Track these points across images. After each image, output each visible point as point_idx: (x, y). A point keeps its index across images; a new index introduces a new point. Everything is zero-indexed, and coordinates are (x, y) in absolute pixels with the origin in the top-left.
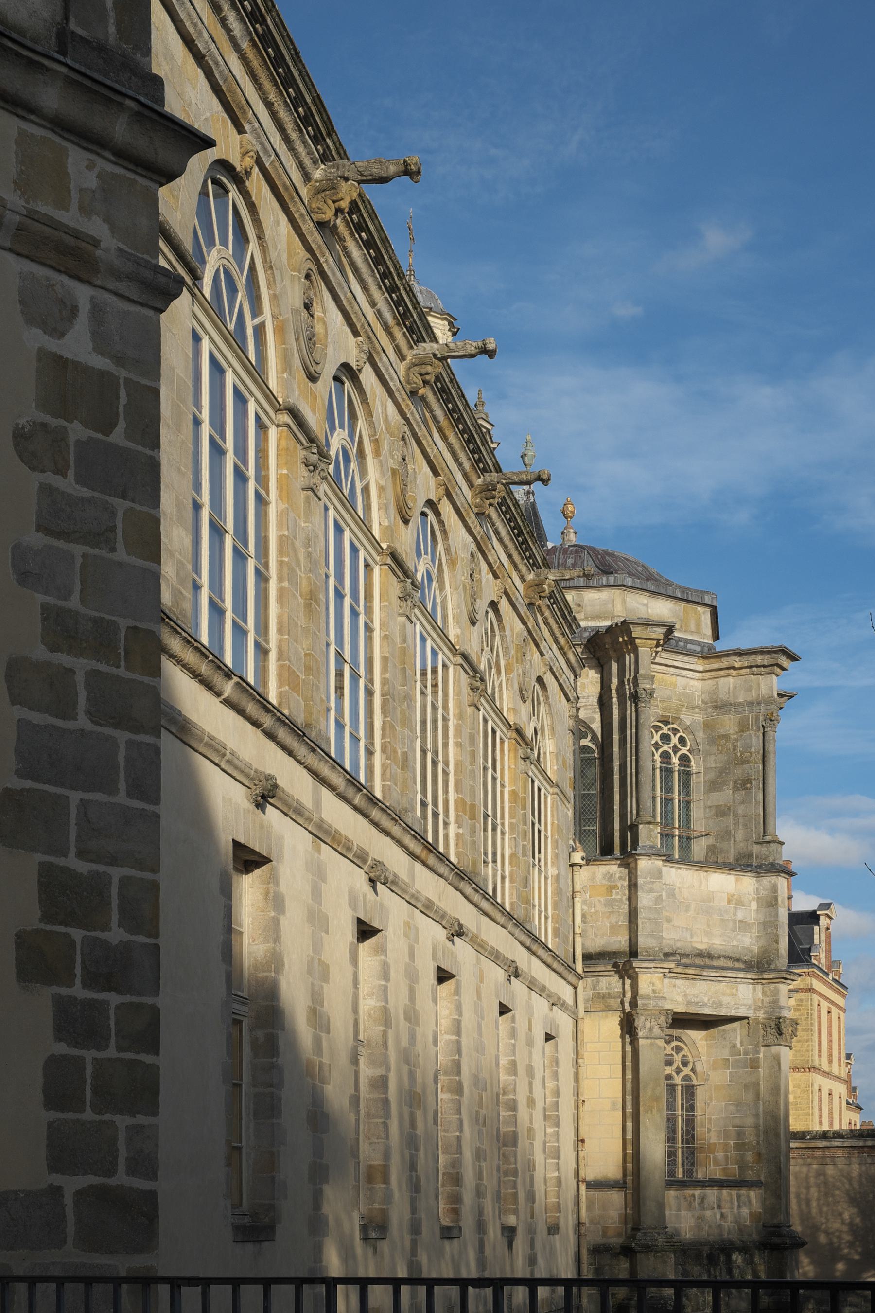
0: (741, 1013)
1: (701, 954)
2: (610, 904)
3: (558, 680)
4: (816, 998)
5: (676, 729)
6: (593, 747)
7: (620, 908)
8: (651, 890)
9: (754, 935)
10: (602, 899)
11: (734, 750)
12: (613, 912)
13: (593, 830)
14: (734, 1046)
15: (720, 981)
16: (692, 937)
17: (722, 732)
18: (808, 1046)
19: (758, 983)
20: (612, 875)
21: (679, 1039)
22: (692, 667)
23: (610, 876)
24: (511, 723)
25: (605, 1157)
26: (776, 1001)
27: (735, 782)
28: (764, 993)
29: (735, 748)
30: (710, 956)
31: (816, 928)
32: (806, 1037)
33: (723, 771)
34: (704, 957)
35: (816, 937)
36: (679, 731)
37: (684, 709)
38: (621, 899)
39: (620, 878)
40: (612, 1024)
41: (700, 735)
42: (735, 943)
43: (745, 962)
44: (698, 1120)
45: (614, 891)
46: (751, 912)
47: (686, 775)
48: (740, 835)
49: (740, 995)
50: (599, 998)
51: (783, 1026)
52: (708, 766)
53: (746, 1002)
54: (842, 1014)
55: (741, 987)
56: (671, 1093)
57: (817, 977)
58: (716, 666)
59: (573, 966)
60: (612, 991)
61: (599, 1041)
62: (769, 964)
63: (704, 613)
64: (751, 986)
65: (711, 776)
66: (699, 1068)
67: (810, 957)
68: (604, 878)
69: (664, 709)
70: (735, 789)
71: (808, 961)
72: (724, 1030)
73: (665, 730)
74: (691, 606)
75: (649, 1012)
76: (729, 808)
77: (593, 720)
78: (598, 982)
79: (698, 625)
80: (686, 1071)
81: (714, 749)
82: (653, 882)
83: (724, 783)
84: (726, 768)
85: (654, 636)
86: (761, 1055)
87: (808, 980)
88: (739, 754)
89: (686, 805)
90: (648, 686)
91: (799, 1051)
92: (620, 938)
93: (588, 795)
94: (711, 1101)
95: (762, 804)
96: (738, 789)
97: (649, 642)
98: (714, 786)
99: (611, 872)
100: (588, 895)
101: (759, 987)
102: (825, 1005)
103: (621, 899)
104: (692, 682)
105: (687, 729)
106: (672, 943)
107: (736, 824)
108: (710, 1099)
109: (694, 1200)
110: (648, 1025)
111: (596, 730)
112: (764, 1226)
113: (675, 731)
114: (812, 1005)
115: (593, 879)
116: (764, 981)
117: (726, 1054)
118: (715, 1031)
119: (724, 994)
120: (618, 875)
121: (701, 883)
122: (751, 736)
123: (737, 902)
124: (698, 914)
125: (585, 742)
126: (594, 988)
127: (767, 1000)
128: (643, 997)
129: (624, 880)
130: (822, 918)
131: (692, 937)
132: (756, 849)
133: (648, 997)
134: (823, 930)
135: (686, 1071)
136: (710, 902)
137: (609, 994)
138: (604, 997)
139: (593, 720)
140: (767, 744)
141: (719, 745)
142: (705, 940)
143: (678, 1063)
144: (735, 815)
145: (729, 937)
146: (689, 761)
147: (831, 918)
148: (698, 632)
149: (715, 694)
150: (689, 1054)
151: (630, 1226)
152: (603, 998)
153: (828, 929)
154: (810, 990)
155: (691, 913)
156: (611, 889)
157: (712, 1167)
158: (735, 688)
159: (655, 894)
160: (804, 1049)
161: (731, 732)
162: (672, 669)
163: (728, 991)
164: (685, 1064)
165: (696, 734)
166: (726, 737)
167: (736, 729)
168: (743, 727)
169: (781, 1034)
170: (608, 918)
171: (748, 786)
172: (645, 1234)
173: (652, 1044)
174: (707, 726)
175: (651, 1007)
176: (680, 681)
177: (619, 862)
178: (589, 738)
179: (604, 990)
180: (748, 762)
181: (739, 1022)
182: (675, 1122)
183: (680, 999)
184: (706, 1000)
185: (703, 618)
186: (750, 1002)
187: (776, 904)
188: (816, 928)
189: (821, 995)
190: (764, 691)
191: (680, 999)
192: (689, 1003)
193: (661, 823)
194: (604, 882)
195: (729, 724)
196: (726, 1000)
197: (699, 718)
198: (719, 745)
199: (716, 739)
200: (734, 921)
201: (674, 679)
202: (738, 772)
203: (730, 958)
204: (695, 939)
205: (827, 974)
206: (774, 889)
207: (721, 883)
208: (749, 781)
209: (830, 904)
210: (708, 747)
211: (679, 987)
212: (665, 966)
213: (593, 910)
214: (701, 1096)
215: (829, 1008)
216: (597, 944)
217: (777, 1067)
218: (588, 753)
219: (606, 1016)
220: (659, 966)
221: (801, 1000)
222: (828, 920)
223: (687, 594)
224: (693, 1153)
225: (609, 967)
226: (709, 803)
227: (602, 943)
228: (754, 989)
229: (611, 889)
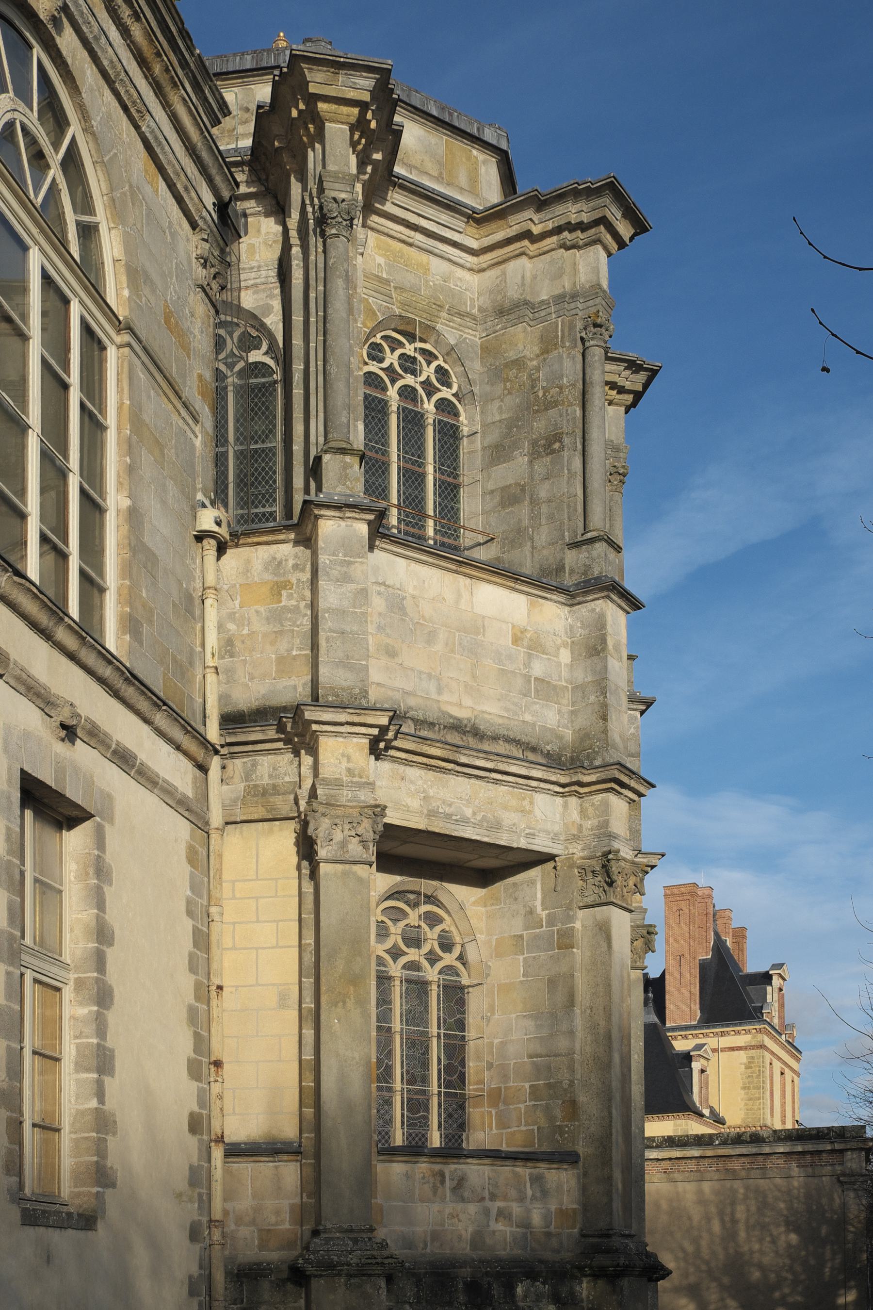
0: (541, 844)
1: (457, 727)
2: (276, 616)
3: (137, 127)
4: (768, 1056)
5: (430, 353)
6: (271, 363)
7: (294, 624)
8: (346, 578)
9: (565, 709)
10: (262, 609)
11: (533, 387)
12: (281, 633)
13: (271, 514)
14: (531, 912)
15: (496, 782)
16: (440, 691)
17: (512, 355)
18: (760, 1104)
19: (571, 794)
20: (280, 563)
21: (430, 899)
22: (456, 237)
23: (277, 565)
24: (121, 318)
25: (258, 1095)
26: (606, 824)
27: (534, 443)
28: (583, 813)
29: (534, 382)
30: (477, 733)
31: (769, 988)
32: (757, 1095)
33: (512, 425)
34: (465, 733)
35: (769, 997)
36: (436, 358)
37: (444, 314)
38: (297, 607)
39: (296, 567)
40: (282, 841)
41: (476, 367)
42: (528, 717)
43: (548, 755)
44: (471, 1047)
45: (284, 593)
46: (561, 663)
47: (449, 436)
48: (543, 536)
49: (538, 813)
50: (255, 795)
51: (614, 868)
52: (489, 420)
53: (549, 827)
54: (796, 1079)
55: (540, 799)
56: (419, 997)
57: (768, 1034)
58: (500, 236)
59: (200, 728)
60: (279, 781)
61: (257, 879)
62: (591, 759)
63: (484, 162)
64: (559, 800)
65: (494, 437)
66: (472, 955)
67: (762, 1014)
68: (266, 569)
69: (404, 305)
70: (534, 455)
71: (759, 1018)
72: (515, 884)
73: (409, 349)
74: (459, 146)
75: (340, 812)
76: (523, 490)
77: (268, 309)
78: (255, 765)
79: (474, 179)
80: (449, 959)
81: (499, 389)
82: (350, 563)
83: (515, 446)
84: (518, 419)
85: (352, 94)
86: (578, 925)
87: (760, 1037)
88: (541, 394)
89: (449, 491)
90: (343, 196)
91: (751, 1109)
92: (294, 681)
93: (263, 450)
94: (493, 1013)
95: (580, 478)
96: (540, 456)
97: (345, 110)
98: (498, 453)
99: (279, 556)
100: (237, 603)
101: (573, 801)
102: (777, 1065)
103: (297, 607)
104: (460, 273)
105: (450, 351)
106: (397, 696)
107: (535, 517)
108: (492, 1009)
109: (443, 1182)
110: (338, 836)
111: (272, 328)
112: (583, 1236)
113: (430, 357)
114: (763, 1062)
115: (247, 571)
116: (582, 790)
117: (517, 926)
118: (499, 887)
119: (505, 808)
120: (291, 563)
121: (459, 596)
122: (560, 357)
123: (532, 644)
124: (453, 651)
125: (256, 356)
126: (247, 777)
127: (588, 824)
128: (327, 782)
129: (303, 570)
130: (775, 978)
131: (440, 691)
132: (571, 558)
133: (338, 783)
134: (776, 990)
135: (449, 959)
136: (478, 634)
137: (274, 786)
138: (261, 793)
139: (268, 309)
140: (588, 371)
141: (507, 380)
142: (467, 702)
143: (431, 942)
144: (534, 502)
145: (516, 704)
146: (457, 415)
147: (784, 979)
148: (473, 191)
149: (499, 292)
150: (453, 929)
151: (308, 1227)
152: (263, 794)
153: (781, 990)
154: (762, 1046)
155: (439, 647)
156: (278, 588)
157: (495, 1131)
158: (535, 277)
159: (353, 586)
160: (756, 1108)
161: (527, 353)
162: (418, 237)
163: (514, 803)
164: (447, 945)
165: (467, 364)
166: (518, 363)
167: (537, 350)
168: (548, 344)
169: (611, 884)
170: (273, 643)
171: (556, 446)
172: (327, 1240)
173: (345, 874)
174: (487, 350)
175: (343, 801)
176: (437, 266)
177: (292, 536)
178: (265, 347)
179: (266, 781)
180: (555, 404)
181: (539, 868)
182: (427, 1050)
183: (415, 803)
184: (468, 812)
185: (482, 170)
186: (557, 828)
187: (604, 649)
188: (769, 988)
189: (773, 1053)
190: (584, 277)
191: (415, 803)
192: (432, 814)
193: (399, 505)
194: (268, 577)
195: (523, 340)
196: (509, 818)
197: (474, 337)
198: (507, 380)
199: (502, 367)
200: (527, 678)
201: (424, 257)
202: (540, 426)
203: (517, 742)
204: (445, 697)
205: (781, 1034)
206: (600, 624)
207: (499, 605)
208: (557, 437)
209: (783, 964)
210: (488, 388)
211: (412, 782)
212: (370, 720)
213: (246, 631)
214: (476, 1003)
215: (782, 1068)
216: (249, 694)
217: (604, 945)
218: (264, 376)
219: (271, 831)
220: (356, 719)
221: (753, 1058)
222: (781, 981)
223: (451, 115)
224: (462, 1107)
225: (272, 734)
226: (490, 486)
227: (263, 692)
228: (566, 806)
229: (278, 588)
